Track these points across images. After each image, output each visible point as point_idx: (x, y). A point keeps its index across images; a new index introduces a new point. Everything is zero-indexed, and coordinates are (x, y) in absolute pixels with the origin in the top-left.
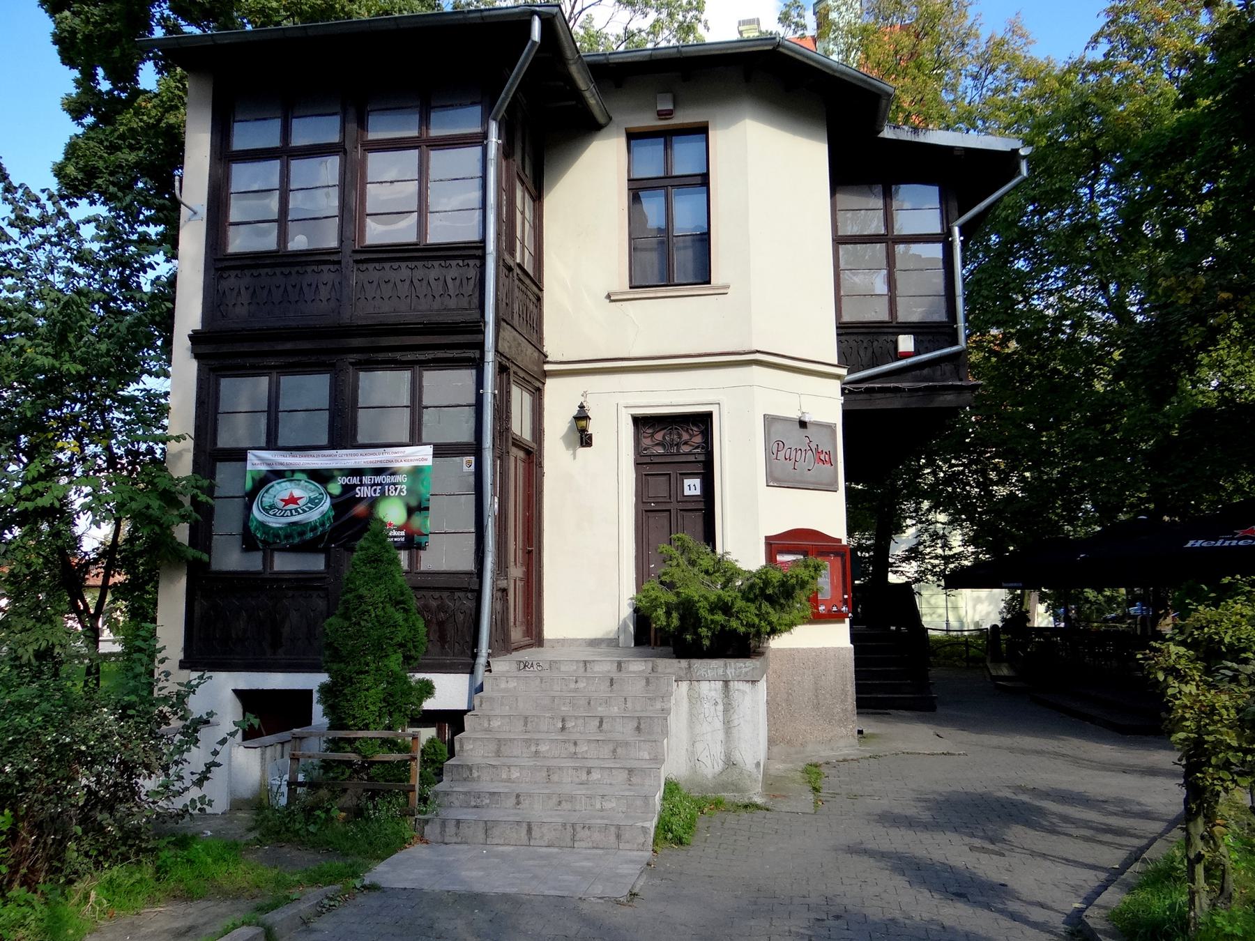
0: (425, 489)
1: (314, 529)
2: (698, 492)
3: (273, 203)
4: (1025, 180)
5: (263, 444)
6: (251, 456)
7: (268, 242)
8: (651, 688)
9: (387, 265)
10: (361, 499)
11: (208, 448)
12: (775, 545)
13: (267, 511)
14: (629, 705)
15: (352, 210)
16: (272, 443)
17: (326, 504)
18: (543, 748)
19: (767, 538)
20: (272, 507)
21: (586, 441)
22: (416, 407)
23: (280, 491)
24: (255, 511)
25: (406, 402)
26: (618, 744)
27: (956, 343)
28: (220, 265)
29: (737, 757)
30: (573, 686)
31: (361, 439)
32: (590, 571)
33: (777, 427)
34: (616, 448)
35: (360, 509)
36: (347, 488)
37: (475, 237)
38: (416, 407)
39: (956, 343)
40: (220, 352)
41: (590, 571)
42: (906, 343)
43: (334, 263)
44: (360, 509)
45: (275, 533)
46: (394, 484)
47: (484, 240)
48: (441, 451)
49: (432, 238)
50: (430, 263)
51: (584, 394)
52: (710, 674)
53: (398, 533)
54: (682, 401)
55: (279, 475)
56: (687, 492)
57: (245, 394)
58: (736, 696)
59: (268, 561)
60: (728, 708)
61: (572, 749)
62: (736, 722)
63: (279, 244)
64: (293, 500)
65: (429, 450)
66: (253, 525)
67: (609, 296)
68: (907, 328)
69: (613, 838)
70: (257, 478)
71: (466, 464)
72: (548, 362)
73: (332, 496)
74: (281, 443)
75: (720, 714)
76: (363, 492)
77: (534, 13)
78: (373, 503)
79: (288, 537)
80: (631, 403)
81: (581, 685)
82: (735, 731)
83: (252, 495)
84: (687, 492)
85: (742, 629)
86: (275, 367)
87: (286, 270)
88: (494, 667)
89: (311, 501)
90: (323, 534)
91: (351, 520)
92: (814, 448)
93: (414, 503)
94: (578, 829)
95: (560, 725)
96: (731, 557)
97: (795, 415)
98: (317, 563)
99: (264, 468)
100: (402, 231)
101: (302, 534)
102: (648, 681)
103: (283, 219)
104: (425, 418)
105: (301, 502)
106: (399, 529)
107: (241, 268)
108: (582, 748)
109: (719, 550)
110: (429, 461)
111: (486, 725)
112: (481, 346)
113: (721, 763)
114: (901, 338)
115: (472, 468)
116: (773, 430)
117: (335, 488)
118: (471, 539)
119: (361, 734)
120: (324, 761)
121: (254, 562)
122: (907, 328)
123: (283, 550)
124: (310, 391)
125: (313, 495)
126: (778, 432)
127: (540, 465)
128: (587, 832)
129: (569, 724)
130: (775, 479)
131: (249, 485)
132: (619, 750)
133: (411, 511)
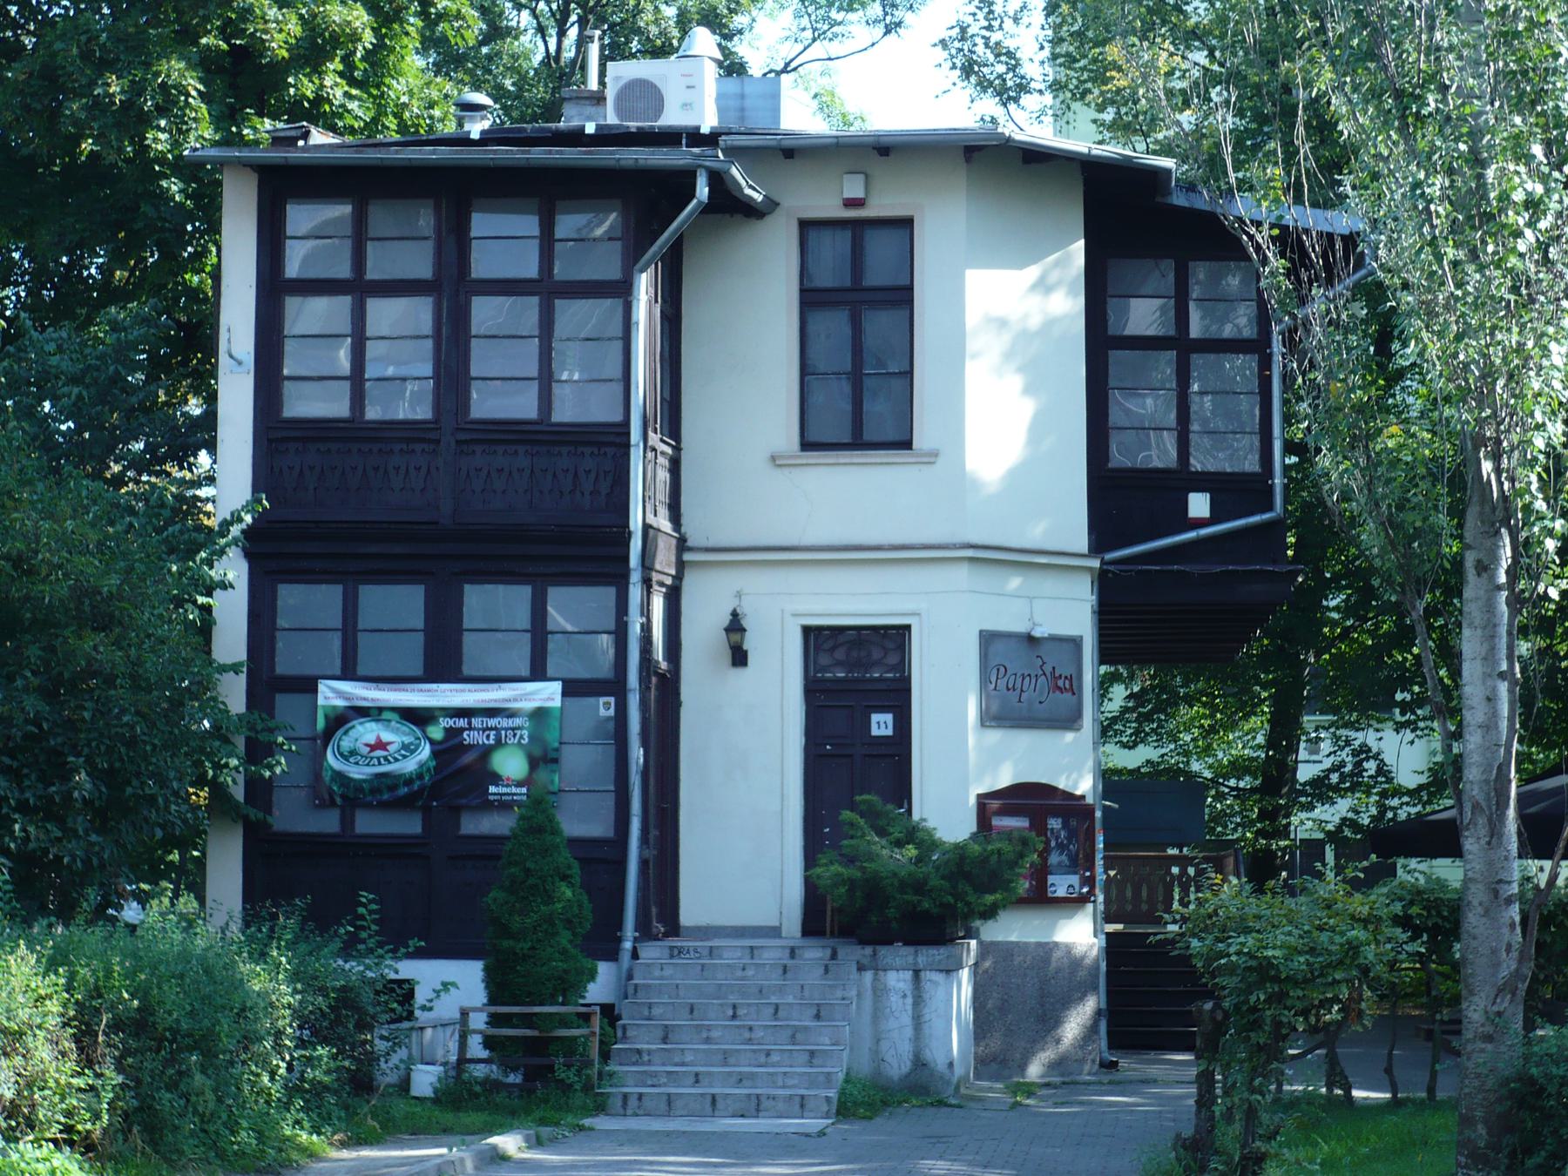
0: (552, 737)
2: (889, 732)
3: (343, 359)
5: (338, 672)
8: (830, 976)
9: (500, 449)
10: (471, 746)
12: (988, 806)
13: (346, 758)
14: (806, 993)
15: (452, 374)
17: (425, 752)
18: (715, 1034)
20: (353, 753)
21: (739, 657)
22: (539, 631)
23: (365, 732)
24: (331, 759)
26: (796, 1029)
27: (1270, 508)
29: (928, 1055)
30: (739, 973)
31: (467, 670)
32: (744, 832)
33: (998, 647)
34: (779, 676)
35: (468, 758)
36: (452, 733)
37: (617, 417)
38: (539, 631)
39: (1270, 508)
40: (275, 550)
41: (744, 832)
42: (1199, 505)
43: (430, 441)
44: (468, 758)
45: (357, 785)
46: (513, 729)
47: (626, 423)
48: (573, 689)
50: (580, 449)
51: (739, 595)
53: (518, 790)
55: (363, 712)
56: (875, 732)
57: (309, 603)
58: (927, 986)
59: (347, 821)
60: (918, 1000)
61: (747, 1035)
62: (927, 1017)
63: (352, 408)
64: (380, 745)
65: (556, 687)
66: (327, 776)
67: (773, 458)
68: (1203, 482)
69: (797, 1107)
70: (332, 715)
71: (605, 707)
72: (690, 549)
73: (432, 742)
74: (361, 671)
75: (909, 1008)
76: (469, 738)
78: (487, 752)
79: (374, 791)
80: (801, 608)
81: (750, 973)
82: (925, 1027)
83: (328, 734)
84: (875, 732)
85: (935, 911)
88: (642, 953)
89: (405, 747)
90: (422, 789)
91: (459, 770)
92: (1048, 669)
93: (537, 752)
94: (763, 1099)
95: (730, 1013)
96: (930, 824)
97: (1020, 627)
98: (409, 825)
99: (340, 703)
100: (521, 405)
101: (393, 788)
102: (827, 970)
103: (357, 376)
104: (550, 646)
105: (391, 748)
106: (519, 784)
108: (759, 1034)
109: (916, 816)
110: (557, 702)
111: (646, 1013)
113: (909, 1064)
115: (612, 712)
117: (436, 732)
118: (610, 801)
119: (537, 1009)
120: (1479, 575)
121: (328, 823)
122: (1203, 482)
123: (368, 806)
124: (397, 606)
125: (407, 740)
127: (677, 693)
128: (771, 1102)
129: (741, 1012)
130: (994, 718)
131: (321, 723)
132: (798, 1036)
133: (534, 763)
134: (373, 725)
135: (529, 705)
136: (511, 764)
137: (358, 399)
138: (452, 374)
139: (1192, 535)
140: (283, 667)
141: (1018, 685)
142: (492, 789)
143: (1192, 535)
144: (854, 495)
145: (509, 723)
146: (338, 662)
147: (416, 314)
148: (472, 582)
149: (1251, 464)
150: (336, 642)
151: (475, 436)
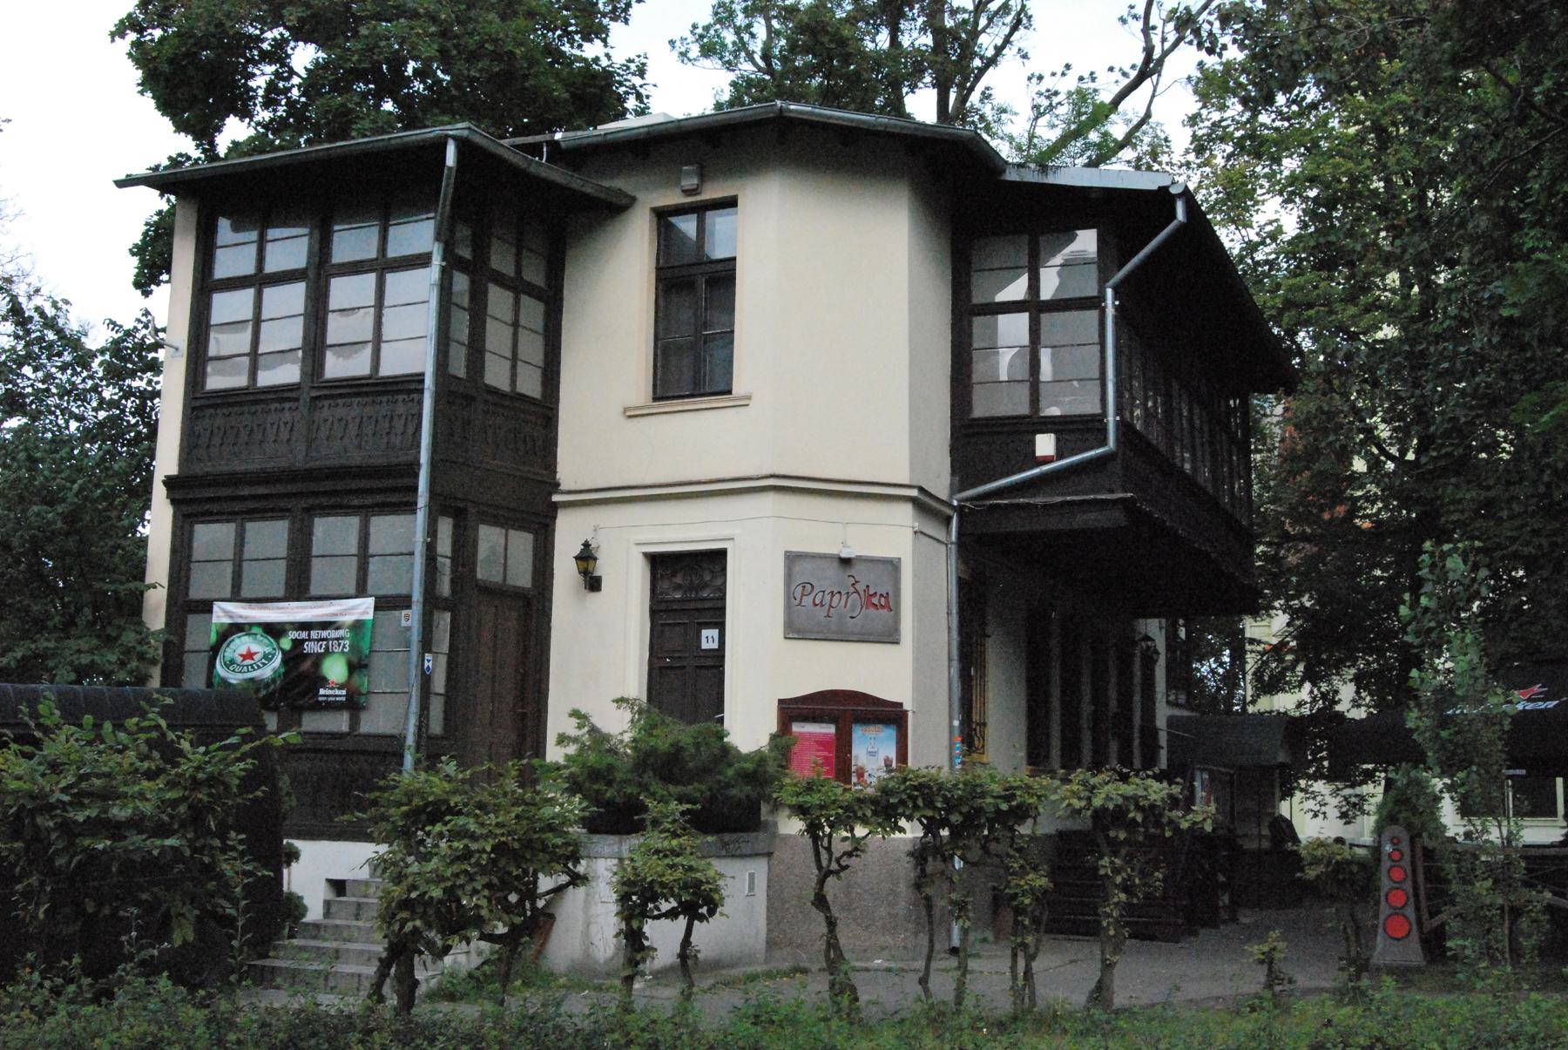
1: (267, 685)
4: (1182, 226)
6: (217, 606)
7: (240, 381)
10: (309, 655)
11: (180, 601)
12: (792, 711)
15: (315, 345)
16: (236, 597)
17: (277, 661)
19: (780, 701)
20: (232, 662)
21: (594, 584)
22: (364, 556)
23: (240, 645)
24: (220, 669)
25: (354, 550)
27: (1104, 442)
28: (197, 403)
36: (297, 644)
42: (1045, 444)
49: (386, 370)
50: (379, 399)
52: (607, 850)
53: (337, 692)
54: (681, 537)
55: (237, 628)
56: (705, 646)
57: (213, 537)
66: (216, 681)
67: (625, 410)
74: (244, 594)
76: (310, 647)
77: (447, 136)
80: (642, 538)
83: (215, 650)
84: (705, 646)
86: (242, 513)
87: (253, 409)
99: (227, 621)
105: (256, 658)
106: (341, 687)
107: (215, 406)
112: (416, 489)
114: (1039, 437)
116: (796, 569)
126: (804, 572)
130: (796, 630)
131: (213, 638)
134: (246, 639)
135: (349, 619)
136: (335, 670)
137: (253, 375)
138: (315, 345)
139: (1036, 471)
140: (196, 593)
141: (828, 598)
142: (322, 692)
143: (1036, 471)
144: (698, 439)
145: (333, 634)
146: (229, 587)
147: (289, 300)
148: (321, 515)
149: (1092, 408)
150: (228, 569)
151: (325, 392)
